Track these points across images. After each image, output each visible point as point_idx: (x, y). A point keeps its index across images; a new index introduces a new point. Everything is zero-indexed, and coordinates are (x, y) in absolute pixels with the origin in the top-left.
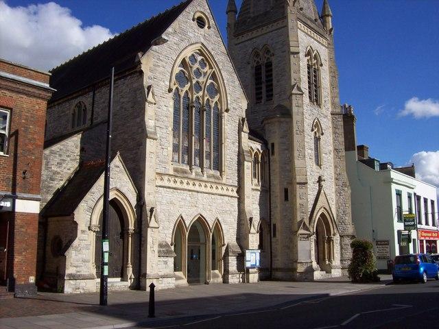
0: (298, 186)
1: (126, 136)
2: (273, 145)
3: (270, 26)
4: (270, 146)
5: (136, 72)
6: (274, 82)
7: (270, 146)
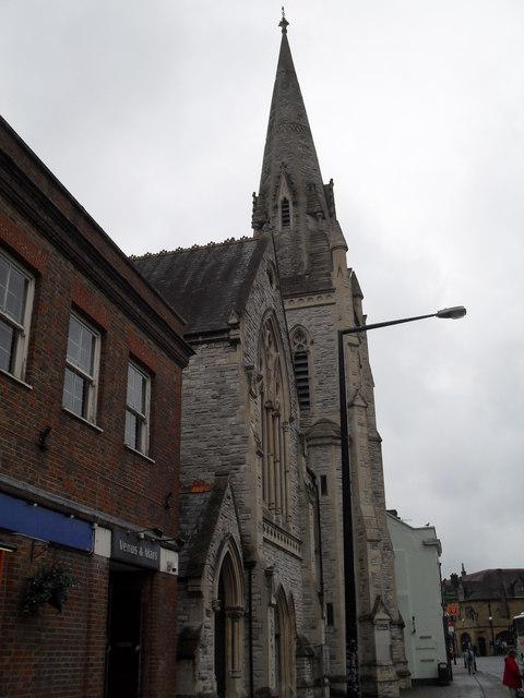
0: (369, 544)
1: (203, 445)
2: (324, 479)
3: (305, 299)
4: (319, 481)
5: (223, 340)
7: (319, 481)
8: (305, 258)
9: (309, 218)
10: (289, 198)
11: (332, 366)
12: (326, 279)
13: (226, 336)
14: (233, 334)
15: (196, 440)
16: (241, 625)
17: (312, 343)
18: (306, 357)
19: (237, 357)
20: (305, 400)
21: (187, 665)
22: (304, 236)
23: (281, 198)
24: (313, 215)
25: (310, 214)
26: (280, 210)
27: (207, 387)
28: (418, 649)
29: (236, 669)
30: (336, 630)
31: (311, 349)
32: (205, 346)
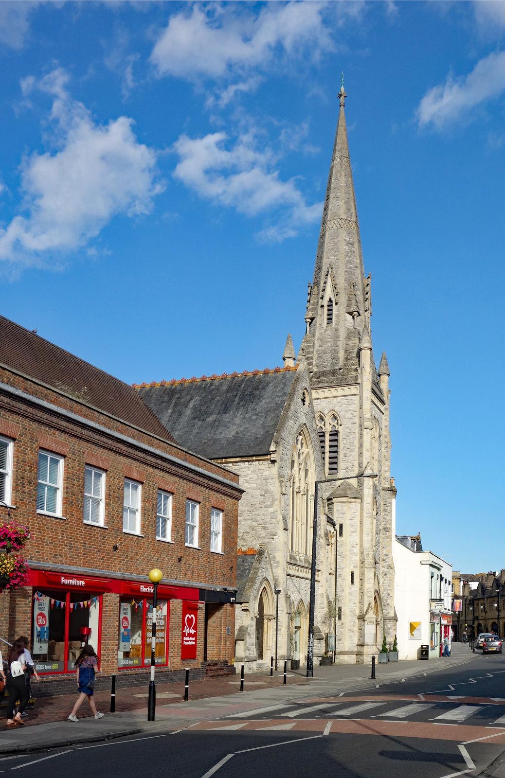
1: (255, 524)
2: (341, 526)
5: (267, 460)
6: (341, 456)
7: (337, 527)
8: (341, 355)
9: (348, 315)
10: (333, 299)
11: (353, 443)
12: (354, 374)
13: (268, 457)
14: (273, 457)
15: (252, 521)
16: (272, 624)
17: (341, 425)
18: (337, 435)
19: (275, 469)
20: (334, 466)
21: (58, 123)
22: (342, 333)
23: (326, 299)
24: (351, 313)
25: (349, 313)
26: (326, 308)
27: (258, 489)
28: (323, 608)
29: (268, 645)
30: (342, 624)
31: (340, 429)
32: (257, 462)
